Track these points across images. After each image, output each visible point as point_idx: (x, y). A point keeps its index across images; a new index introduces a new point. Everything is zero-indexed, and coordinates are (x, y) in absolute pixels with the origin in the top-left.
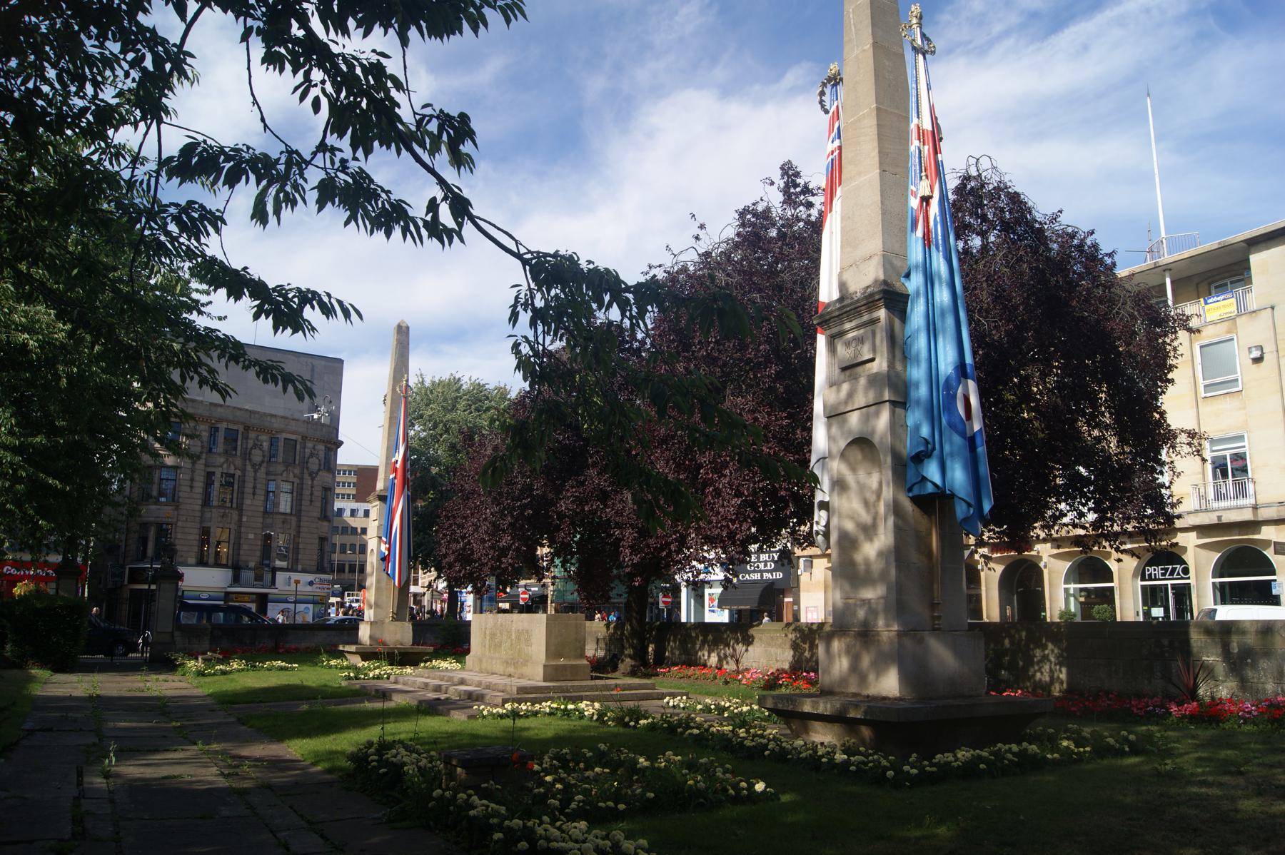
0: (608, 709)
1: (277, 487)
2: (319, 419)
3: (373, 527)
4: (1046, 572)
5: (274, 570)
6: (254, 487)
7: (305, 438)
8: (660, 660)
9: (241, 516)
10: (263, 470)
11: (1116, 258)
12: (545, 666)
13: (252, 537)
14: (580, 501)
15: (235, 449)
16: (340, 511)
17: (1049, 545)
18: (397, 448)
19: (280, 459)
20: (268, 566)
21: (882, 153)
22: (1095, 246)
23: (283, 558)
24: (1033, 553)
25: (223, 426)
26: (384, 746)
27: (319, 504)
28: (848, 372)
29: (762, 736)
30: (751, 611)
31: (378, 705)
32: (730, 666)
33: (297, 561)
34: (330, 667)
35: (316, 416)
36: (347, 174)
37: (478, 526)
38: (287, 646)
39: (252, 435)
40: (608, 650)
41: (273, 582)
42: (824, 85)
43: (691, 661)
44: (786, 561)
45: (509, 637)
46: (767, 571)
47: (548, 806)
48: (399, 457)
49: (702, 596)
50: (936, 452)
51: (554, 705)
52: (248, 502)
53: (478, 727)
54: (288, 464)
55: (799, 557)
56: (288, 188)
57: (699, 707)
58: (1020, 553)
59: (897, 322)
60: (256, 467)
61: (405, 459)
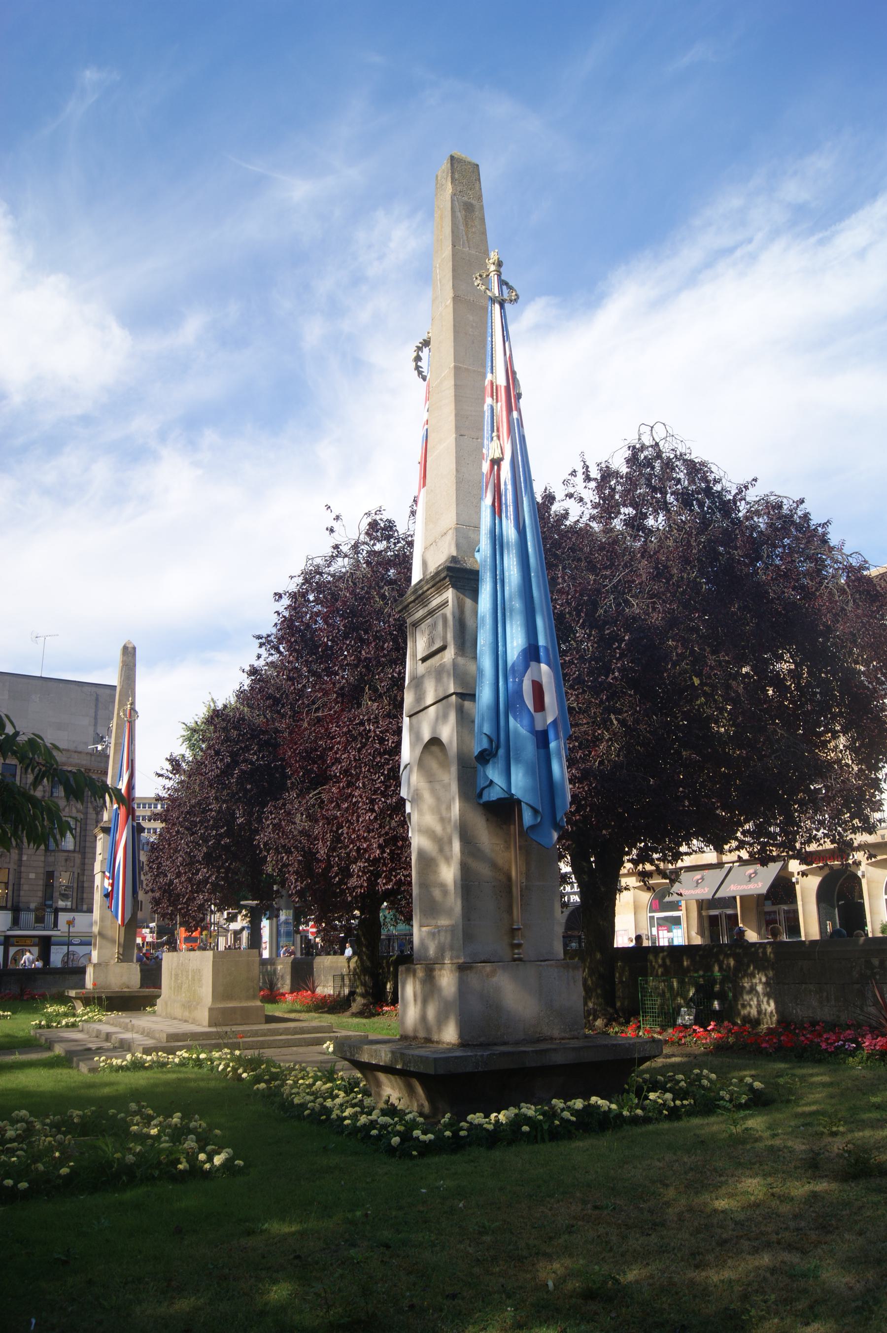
4: (798, 887)
5: (57, 911)
11: (830, 529)
12: (210, 1010)
18: (121, 776)
20: (50, 906)
22: (806, 517)
23: (64, 897)
35: (100, 748)
41: (56, 924)
42: (419, 349)
45: (187, 978)
50: (501, 752)
59: (468, 602)
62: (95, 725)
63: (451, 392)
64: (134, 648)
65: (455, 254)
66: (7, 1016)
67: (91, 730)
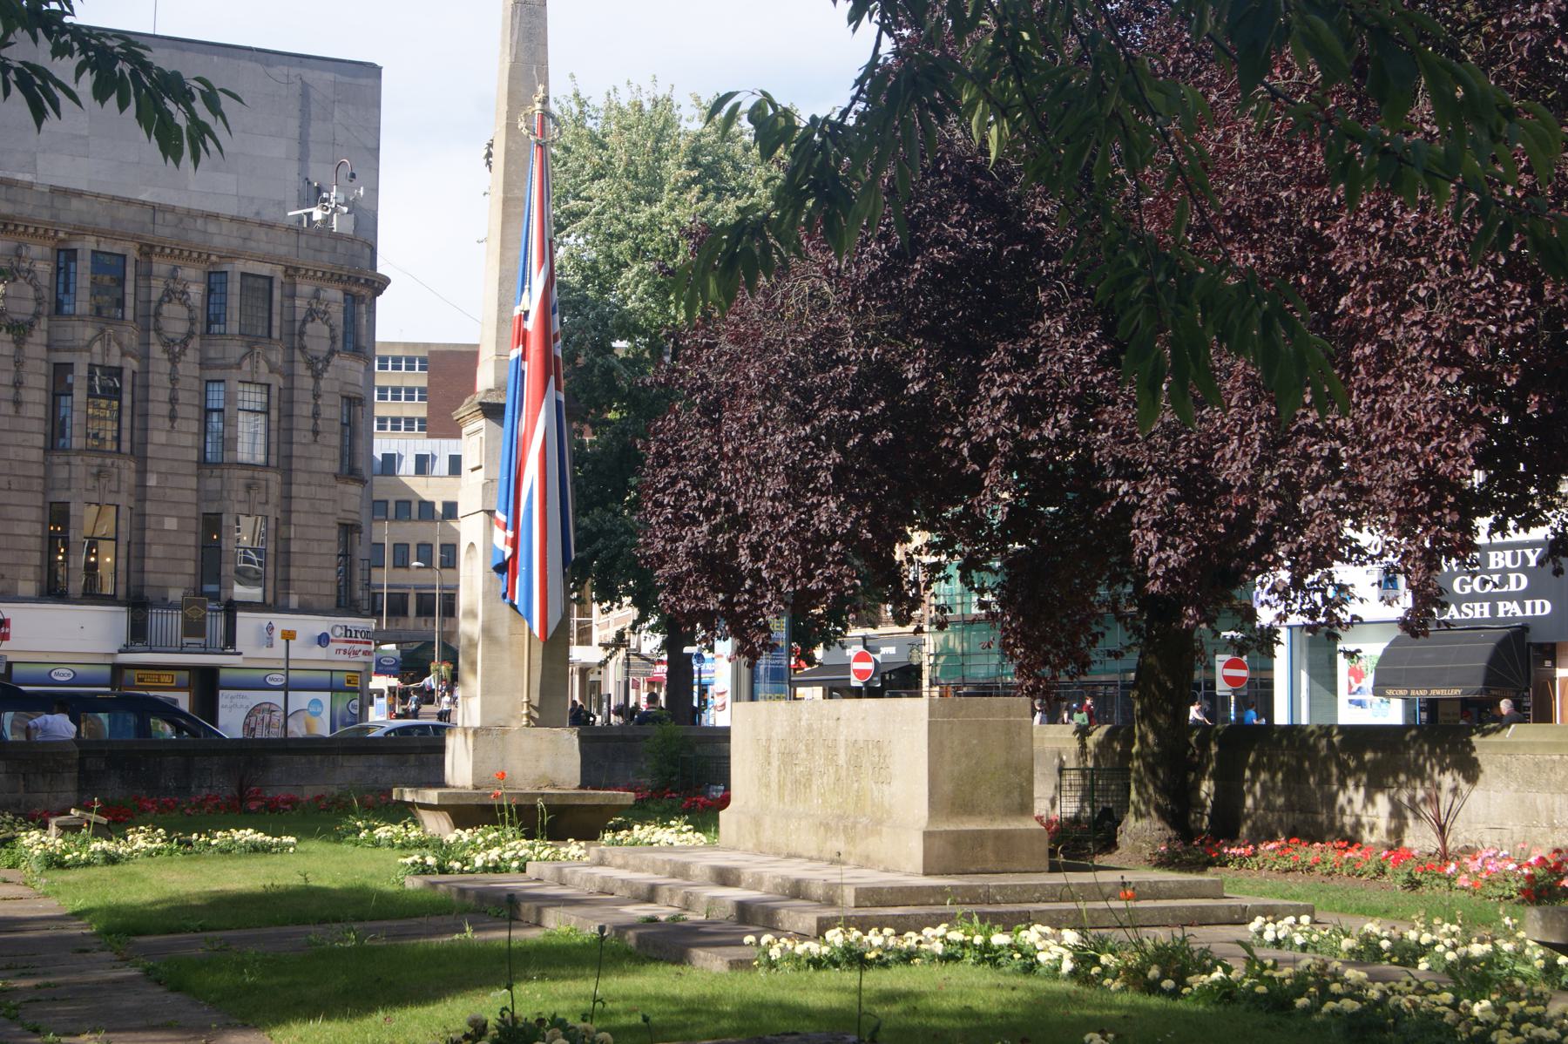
5: (231, 608)
8: (1227, 825)
12: (928, 835)
18: (525, 279)
20: (215, 597)
23: (244, 577)
32: (1420, 838)
35: (318, 214)
40: (1088, 794)
43: (1312, 822)
45: (831, 759)
46: (1509, 597)
51: (956, 936)
57: (1346, 943)
62: (303, 158)
66: (288, 845)
67: (292, 172)
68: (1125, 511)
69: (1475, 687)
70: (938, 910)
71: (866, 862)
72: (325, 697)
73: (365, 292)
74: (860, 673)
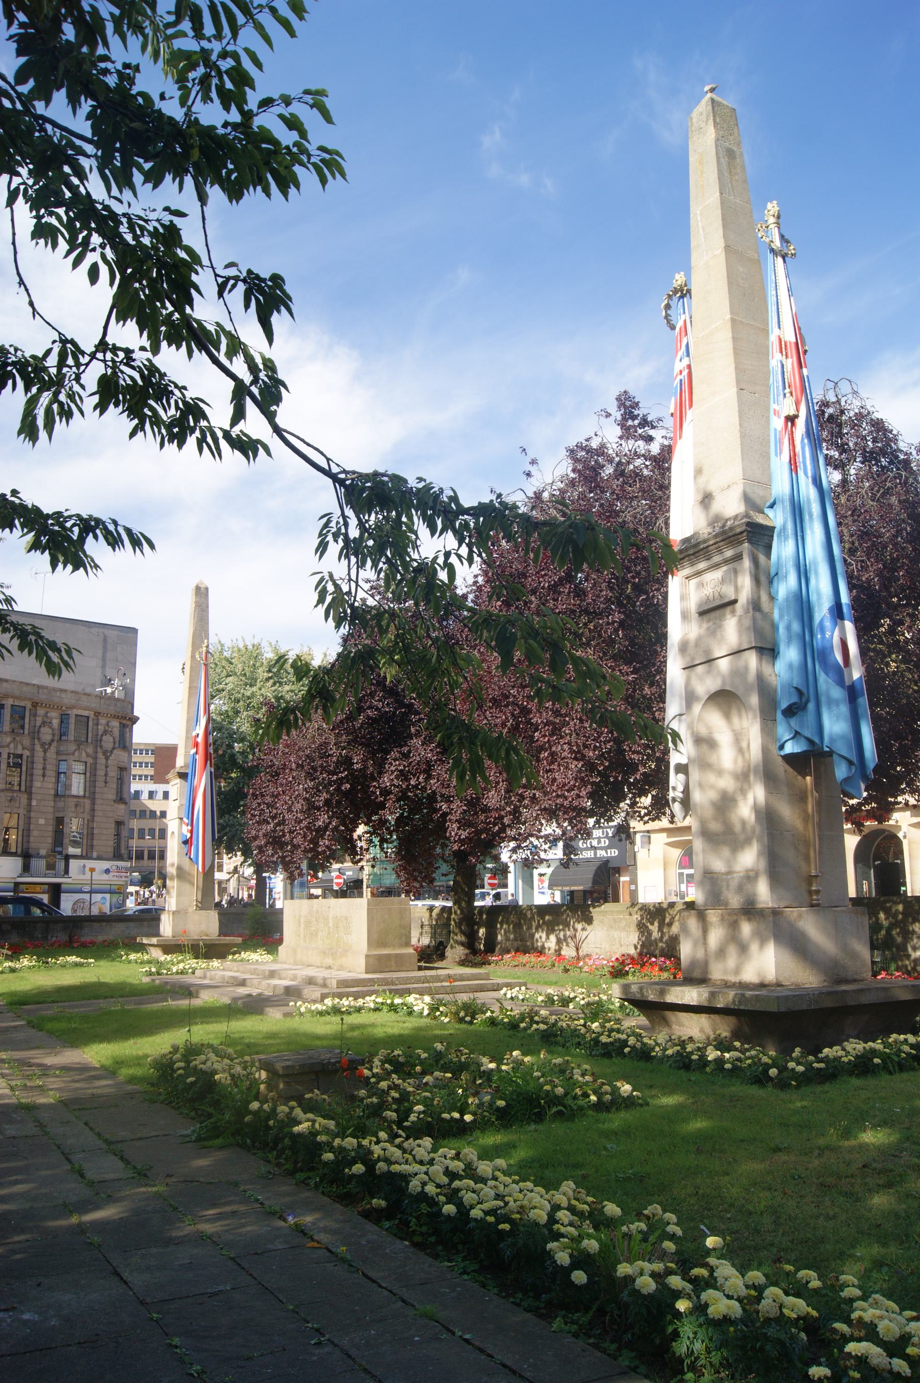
0: (440, 1003)
1: (69, 767)
2: (113, 693)
3: (173, 809)
4: (905, 844)
5: (67, 858)
6: (44, 769)
7: (97, 714)
8: (491, 947)
9: (30, 799)
10: (53, 749)
12: (367, 956)
13: (43, 823)
14: (403, 775)
15: (23, 727)
16: (137, 794)
17: (908, 813)
19: (72, 738)
20: (60, 853)
21: (739, 370)
23: (75, 844)
24: (891, 822)
25: (9, 702)
26: (192, 1051)
27: (115, 786)
28: (705, 617)
29: (618, 1031)
30: (585, 892)
31: (184, 1003)
33: (91, 847)
34: (130, 962)
35: (109, 690)
36: (133, 368)
37: (291, 801)
38: (83, 939)
39: (41, 711)
40: (434, 935)
41: (67, 871)
44: (623, 836)
46: (601, 848)
47: (385, 1119)
48: (200, 730)
49: (532, 876)
50: (811, 706)
51: (380, 1000)
52: (37, 784)
53: (295, 1024)
54: (80, 743)
55: (635, 833)
56: (62, 397)
57: (540, 998)
58: (880, 822)
59: (762, 558)
60: (45, 747)
61: (207, 733)
62: (104, 667)
63: (729, 345)
64: (207, 589)
65: (723, 202)
68: (445, 815)
69: (588, 886)
70: (372, 988)
71: (341, 968)
72: (108, 896)
73: (129, 723)
74: (338, 884)
